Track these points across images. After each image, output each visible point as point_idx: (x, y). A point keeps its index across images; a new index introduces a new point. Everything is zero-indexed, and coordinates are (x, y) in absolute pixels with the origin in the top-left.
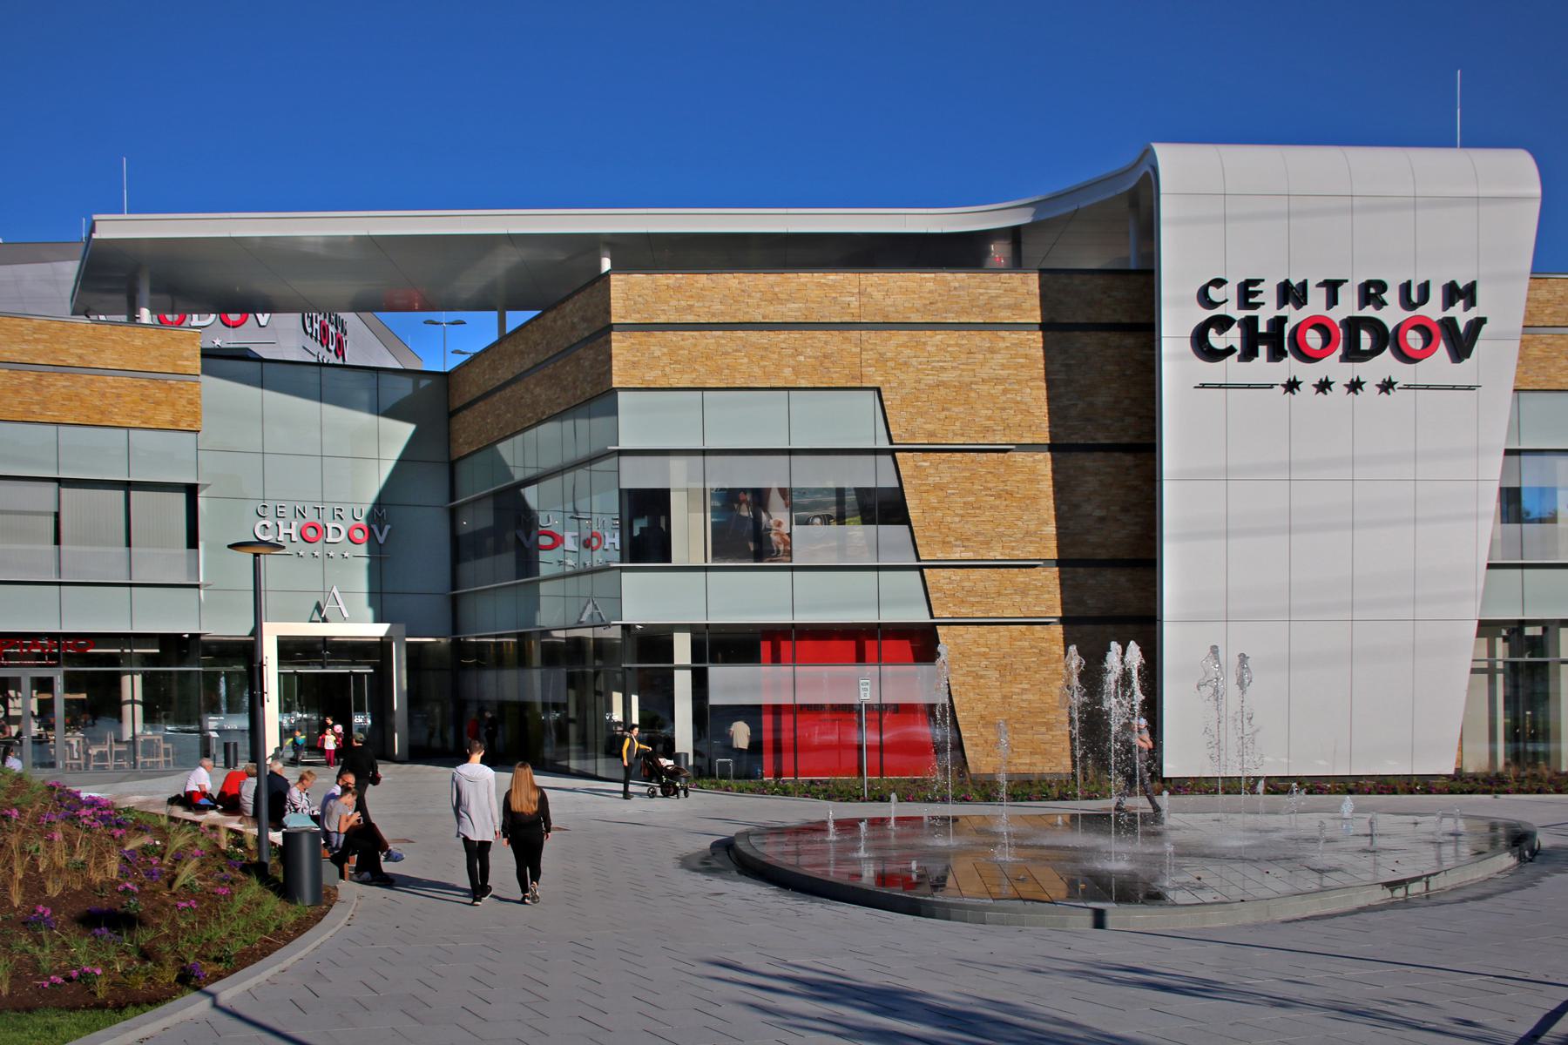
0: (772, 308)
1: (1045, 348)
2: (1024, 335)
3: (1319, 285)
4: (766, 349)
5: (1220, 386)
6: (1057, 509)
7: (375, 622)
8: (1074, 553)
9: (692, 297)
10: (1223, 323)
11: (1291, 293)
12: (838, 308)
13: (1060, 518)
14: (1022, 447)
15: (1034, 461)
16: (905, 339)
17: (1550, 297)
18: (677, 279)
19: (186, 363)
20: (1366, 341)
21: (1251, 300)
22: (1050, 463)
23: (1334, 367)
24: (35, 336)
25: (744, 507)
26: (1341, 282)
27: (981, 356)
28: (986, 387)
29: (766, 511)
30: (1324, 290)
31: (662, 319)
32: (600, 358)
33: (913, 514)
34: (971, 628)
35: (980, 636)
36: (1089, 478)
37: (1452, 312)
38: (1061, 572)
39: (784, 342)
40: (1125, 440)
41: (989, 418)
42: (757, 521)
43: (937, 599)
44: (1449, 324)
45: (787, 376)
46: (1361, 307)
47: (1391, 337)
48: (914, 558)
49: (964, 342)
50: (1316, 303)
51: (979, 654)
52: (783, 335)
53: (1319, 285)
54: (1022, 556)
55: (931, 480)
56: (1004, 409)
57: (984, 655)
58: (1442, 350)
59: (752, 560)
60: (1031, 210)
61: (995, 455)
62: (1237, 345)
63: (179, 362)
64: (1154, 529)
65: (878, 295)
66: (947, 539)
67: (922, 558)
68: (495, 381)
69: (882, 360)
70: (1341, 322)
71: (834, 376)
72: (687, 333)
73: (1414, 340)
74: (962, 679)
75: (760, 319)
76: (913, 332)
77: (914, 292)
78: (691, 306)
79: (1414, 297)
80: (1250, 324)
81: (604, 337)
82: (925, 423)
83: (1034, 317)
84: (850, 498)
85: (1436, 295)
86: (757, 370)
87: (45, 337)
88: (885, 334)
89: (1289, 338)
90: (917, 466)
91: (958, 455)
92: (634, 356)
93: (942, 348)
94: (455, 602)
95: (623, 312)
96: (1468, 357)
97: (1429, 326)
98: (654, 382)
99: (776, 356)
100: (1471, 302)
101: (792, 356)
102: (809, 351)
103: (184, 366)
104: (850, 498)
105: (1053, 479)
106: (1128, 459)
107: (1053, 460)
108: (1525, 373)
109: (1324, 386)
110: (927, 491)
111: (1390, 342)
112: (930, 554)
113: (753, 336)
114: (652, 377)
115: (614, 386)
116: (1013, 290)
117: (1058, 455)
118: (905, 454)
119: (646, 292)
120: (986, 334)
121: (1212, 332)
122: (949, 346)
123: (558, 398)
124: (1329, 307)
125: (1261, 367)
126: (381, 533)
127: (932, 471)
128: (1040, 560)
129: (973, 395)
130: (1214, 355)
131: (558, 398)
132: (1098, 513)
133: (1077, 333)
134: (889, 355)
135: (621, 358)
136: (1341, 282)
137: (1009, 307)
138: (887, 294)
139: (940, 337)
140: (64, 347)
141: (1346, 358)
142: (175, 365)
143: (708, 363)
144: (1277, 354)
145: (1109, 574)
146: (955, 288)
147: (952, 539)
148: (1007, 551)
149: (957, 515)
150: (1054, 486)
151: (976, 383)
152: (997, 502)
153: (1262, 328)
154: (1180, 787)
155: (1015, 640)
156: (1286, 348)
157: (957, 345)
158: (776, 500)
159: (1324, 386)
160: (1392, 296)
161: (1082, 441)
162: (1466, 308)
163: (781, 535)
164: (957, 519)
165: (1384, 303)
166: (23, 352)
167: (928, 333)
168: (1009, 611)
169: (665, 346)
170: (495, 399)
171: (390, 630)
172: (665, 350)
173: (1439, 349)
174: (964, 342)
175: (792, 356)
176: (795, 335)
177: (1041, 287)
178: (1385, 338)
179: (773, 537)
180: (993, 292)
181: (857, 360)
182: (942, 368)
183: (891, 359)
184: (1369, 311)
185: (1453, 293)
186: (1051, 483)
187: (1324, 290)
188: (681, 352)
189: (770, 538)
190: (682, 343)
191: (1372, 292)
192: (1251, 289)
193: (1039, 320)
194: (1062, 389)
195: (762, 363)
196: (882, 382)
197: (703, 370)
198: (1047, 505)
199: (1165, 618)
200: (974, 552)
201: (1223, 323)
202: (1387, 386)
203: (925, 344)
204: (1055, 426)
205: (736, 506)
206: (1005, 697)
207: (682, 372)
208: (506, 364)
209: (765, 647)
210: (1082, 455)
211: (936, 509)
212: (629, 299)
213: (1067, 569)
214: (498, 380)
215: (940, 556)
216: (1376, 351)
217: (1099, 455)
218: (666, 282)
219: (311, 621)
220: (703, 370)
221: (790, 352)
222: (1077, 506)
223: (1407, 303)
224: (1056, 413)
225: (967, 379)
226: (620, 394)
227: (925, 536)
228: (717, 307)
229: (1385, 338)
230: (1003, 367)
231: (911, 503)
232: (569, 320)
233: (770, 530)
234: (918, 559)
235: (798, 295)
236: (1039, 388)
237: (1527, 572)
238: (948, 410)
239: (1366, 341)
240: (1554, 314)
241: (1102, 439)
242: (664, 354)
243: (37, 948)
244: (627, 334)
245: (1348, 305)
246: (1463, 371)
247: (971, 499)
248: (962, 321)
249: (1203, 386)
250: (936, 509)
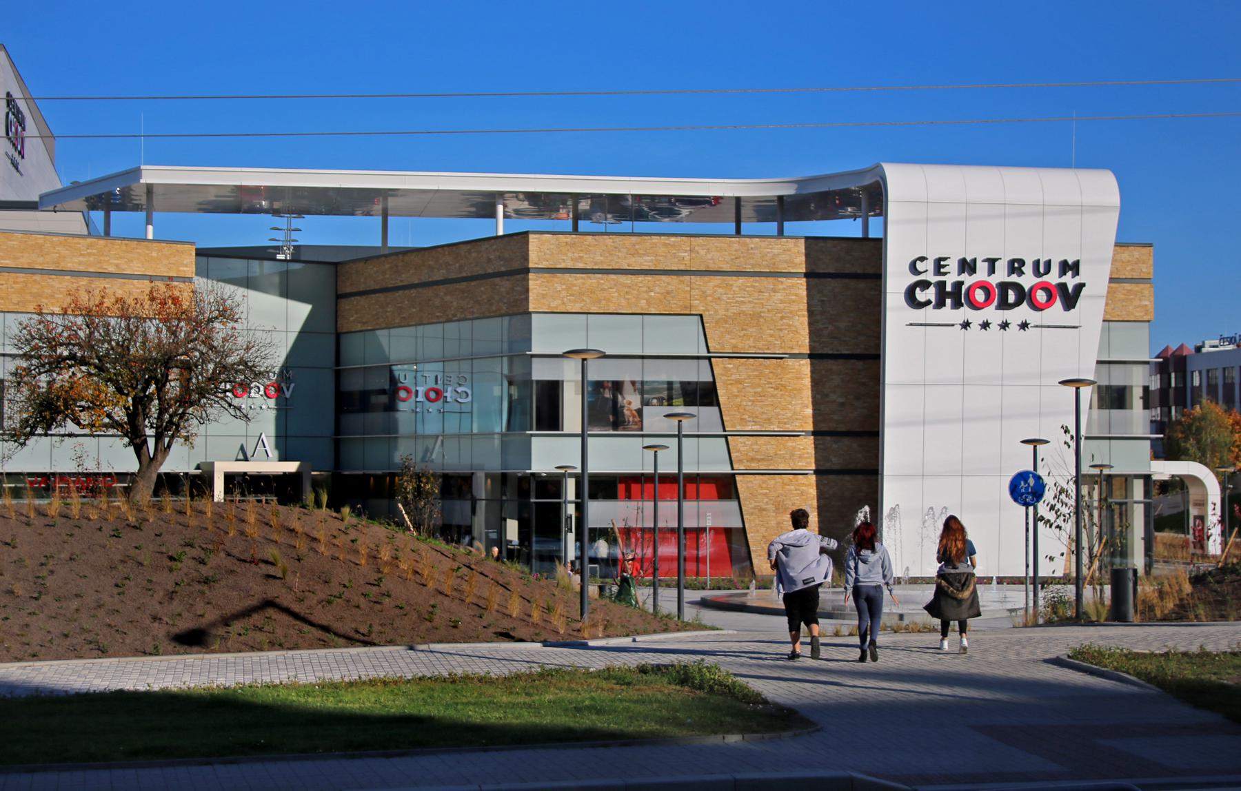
0: (634, 260)
1: (808, 289)
2: (795, 281)
3: (984, 261)
4: (629, 287)
5: (921, 325)
6: (813, 397)
7: (280, 461)
8: (824, 427)
9: (582, 251)
10: (925, 285)
11: (967, 266)
12: (676, 260)
13: (815, 403)
14: (793, 356)
15: (800, 365)
16: (719, 282)
17: (1130, 259)
18: (573, 238)
19: (185, 269)
20: (1012, 297)
21: (942, 270)
22: (809, 366)
23: (992, 314)
24: (89, 251)
25: (607, 391)
26: (997, 260)
27: (767, 294)
28: (770, 315)
29: (621, 394)
30: (986, 264)
31: (562, 266)
32: (516, 289)
33: (721, 399)
34: (757, 476)
35: (764, 482)
36: (834, 377)
37: (1064, 279)
38: (815, 440)
39: (641, 283)
40: (858, 351)
41: (771, 336)
42: (615, 401)
43: (737, 457)
44: (1063, 286)
45: (643, 305)
46: (1009, 275)
47: (1027, 294)
48: (722, 429)
49: (757, 284)
50: (981, 274)
51: (762, 494)
52: (641, 278)
53: (984, 261)
54: (791, 429)
55: (733, 377)
56: (781, 330)
57: (765, 494)
58: (1058, 304)
59: (611, 428)
60: (795, 186)
61: (775, 361)
62: (933, 300)
63: (181, 269)
64: (878, 412)
65: (702, 252)
66: (744, 417)
67: (727, 429)
68: (398, 281)
69: (704, 295)
70: (997, 285)
71: (673, 306)
72: (578, 275)
73: (1041, 296)
74: (751, 510)
75: (626, 267)
76: (725, 278)
77: (725, 250)
78: (581, 257)
79: (1042, 270)
80: (941, 285)
81: (523, 276)
82: (731, 339)
83: (802, 268)
84: (677, 386)
85: (1055, 269)
86: (623, 302)
87: (94, 251)
88: (706, 278)
89: (965, 294)
90: (725, 368)
91: (751, 361)
92: (543, 290)
93: (742, 289)
94: (337, 444)
95: (536, 260)
96: (1074, 307)
97: (1051, 289)
98: (556, 308)
99: (635, 292)
100: (1076, 273)
101: (646, 292)
102: (657, 289)
103: (184, 271)
104: (677, 386)
105: (812, 377)
106: (859, 364)
107: (812, 364)
108: (1113, 309)
109: (985, 325)
110: (731, 384)
111: (1027, 297)
112: (732, 427)
113: (622, 279)
114: (555, 305)
115: (530, 310)
116: (789, 250)
117: (815, 361)
118: (718, 359)
119: (552, 247)
120: (770, 280)
121: (918, 290)
122: (747, 287)
123: (472, 307)
124: (989, 275)
125: (947, 313)
126: (288, 390)
127: (735, 371)
128: (802, 431)
129: (761, 320)
131: (472, 307)
132: (840, 400)
133: (829, 280)
134: (709, 292)
135: (535, 291)
136: (997, 260)
137: (786, 262)
138: (708, 251)
139: (741, 280)
140: (107, 258)
141: (1000, 307)
142: (179, 271)
143: (592, 295)
144: (957, 305)
145: (846, 441)
146: (752, 248)
147: (747, 417)
148: (781, 425)
149: (750, 401)
150: (812, 382)
151: (764, 312)
152: (776, 392)
153: (949, 288)
155: (786, 485)
156: (963, 301)
157: (752, 286)
158: (628, 388)
159: (985, 325)
160: (1028, 269)
161: (830, 352)
162: (1073, 277)
163: (631, 411)
164: (750, 403)
165: (1023, 273)
166: (80, 263)
167: (734, 278)
168: (783, 465)
169: (564, 284)
170: (397, 294)
171: (300, 467)
172: (564, 287)
174: (757, 284)
175: (646, 292)
176: (649, 278)
177: (806, 249)
178: (1024, 296)
179: (626, 412)
180: (776, 251)
181: (688, 296)
182: (742, 301)
183: (710, 295)
184: (1014, 278)
185: (1065, 267)
186: (809, 380)
187: (986, 264)
188: (575, 288)
189: (623, 412)
190: (575, 282)
191: (1016, 266)
192: (942, 263)
193: (804, 271)
194: (818, 317)
195: (627, 297)
196: (704, 311)
197: (588, 300)
198: (807, 394)
199: (886, 472)
200: (760, 425)
201: (925, 285)
202: (1024, 326)
203: (732, 285)
204: (814, 342)
205: (602, 390)
206: (778, 523)
207: (575, 302)
208: (411, 271)
209: (621, 488)
210: (830, 361)
211: (737, 396)
212: (541, 251)
213: (819, 437)
214: (401, 281)
215: (739, 428)
216: (1018, 303)
217: (841, 361)
218: (565, 240)
219: (237, 460)
220: (588, 300)
221: (644, 289)
222: (827, 395)
223: (1037, 273)
224: (814, 333)
225: (759, 310)
226: (533, 315)
227: (729, 415)
228: (598, 258)
229: (1024, 296)
230: (782, 302)
231: (720, 392)
232: (485, 256)
233: (624, 407)
234: (725, 430)
235: (651, 251)
236: (804, 316)
237: (1112, 441)
238: (746, 330)
239: (1012, 297)
240: (1132, 270)
241: (844, 351)
242: (563, 289)
244: (540, 275)
245: (1001, 275)
246: (1071, 317)
247: (759, 390)
248: (756, 270)
249: (911, 325)
250: (737, 396)
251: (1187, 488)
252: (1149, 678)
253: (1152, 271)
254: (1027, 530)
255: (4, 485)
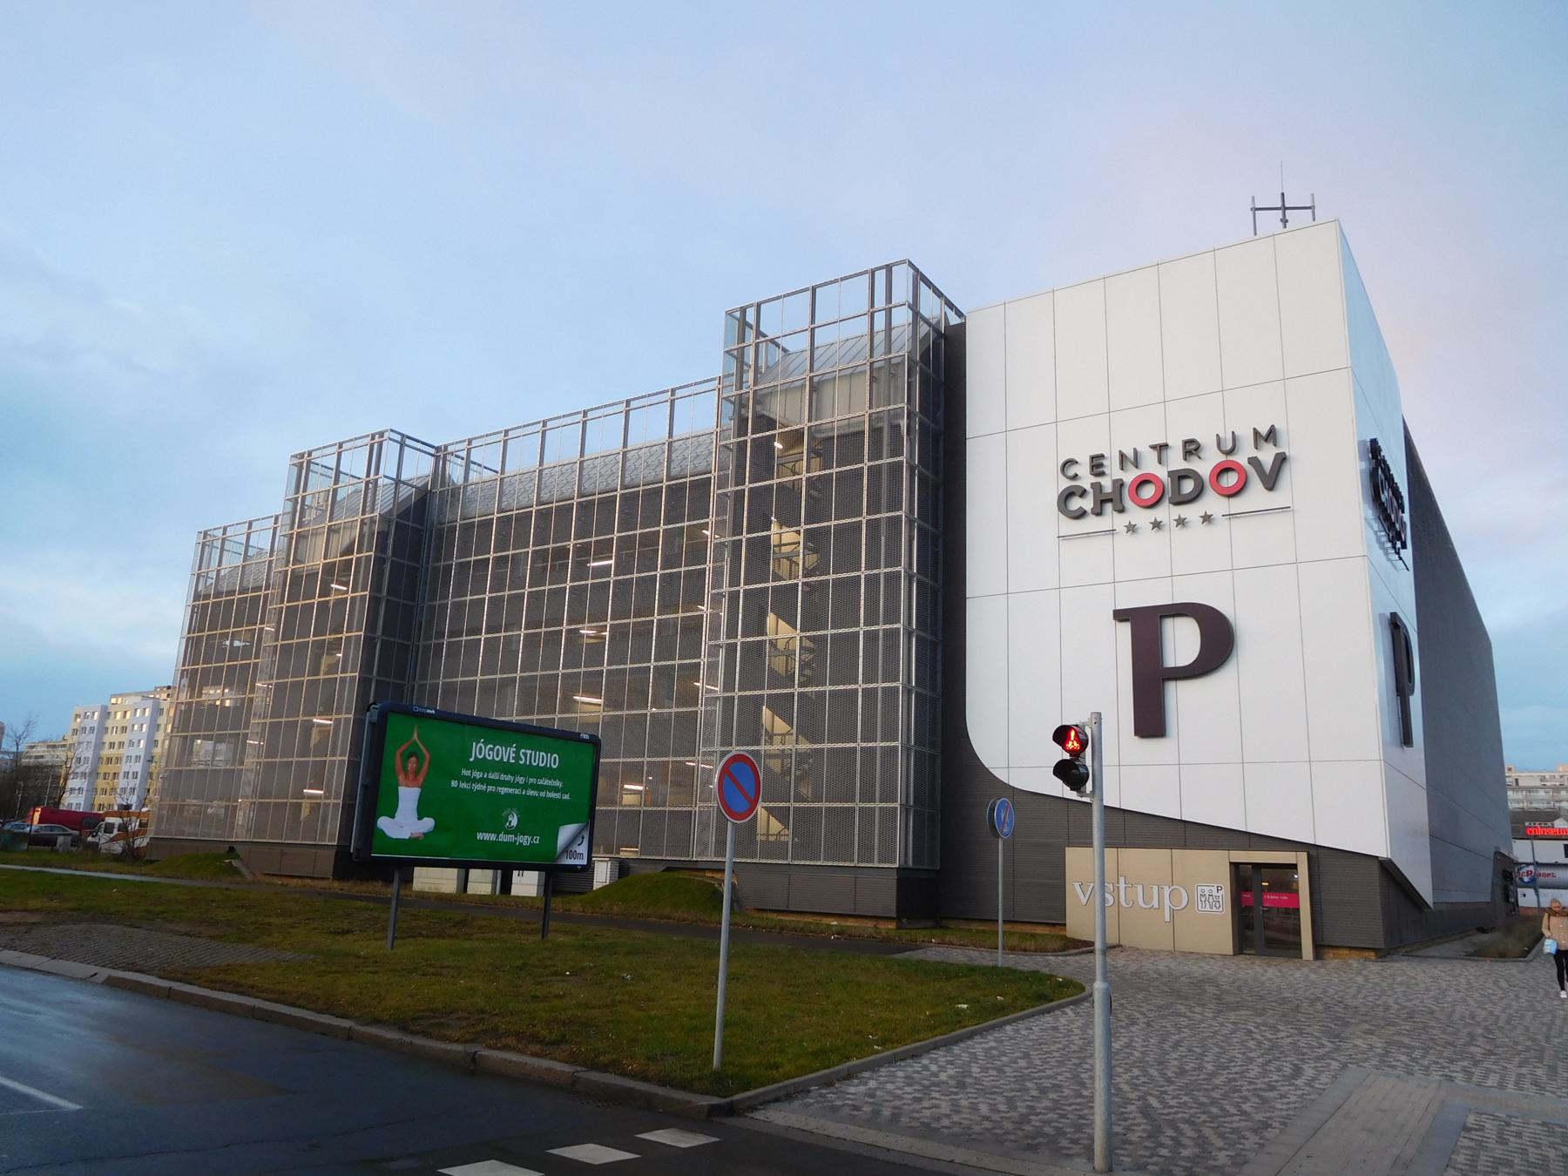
80: (1097, 488)
125: (1111, 519)
130: (1081, 515)
154: (666, 1055)
173: (1063, 488)
243: (774, 1072)
245: (1176, 461)
251: (1462, 938)
252: (948, 928)
253: (65, 809)
254: (423, 443)
255: (332, 585)
